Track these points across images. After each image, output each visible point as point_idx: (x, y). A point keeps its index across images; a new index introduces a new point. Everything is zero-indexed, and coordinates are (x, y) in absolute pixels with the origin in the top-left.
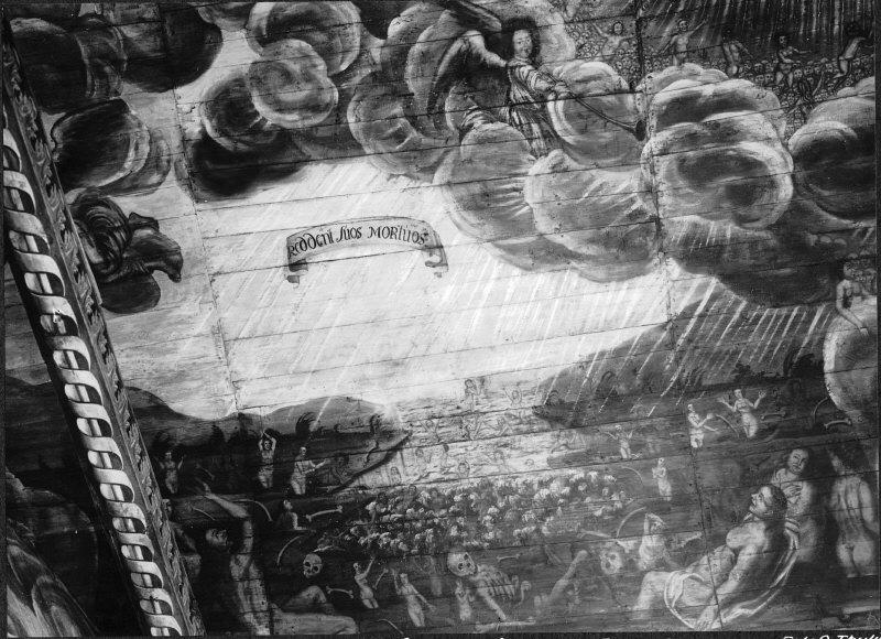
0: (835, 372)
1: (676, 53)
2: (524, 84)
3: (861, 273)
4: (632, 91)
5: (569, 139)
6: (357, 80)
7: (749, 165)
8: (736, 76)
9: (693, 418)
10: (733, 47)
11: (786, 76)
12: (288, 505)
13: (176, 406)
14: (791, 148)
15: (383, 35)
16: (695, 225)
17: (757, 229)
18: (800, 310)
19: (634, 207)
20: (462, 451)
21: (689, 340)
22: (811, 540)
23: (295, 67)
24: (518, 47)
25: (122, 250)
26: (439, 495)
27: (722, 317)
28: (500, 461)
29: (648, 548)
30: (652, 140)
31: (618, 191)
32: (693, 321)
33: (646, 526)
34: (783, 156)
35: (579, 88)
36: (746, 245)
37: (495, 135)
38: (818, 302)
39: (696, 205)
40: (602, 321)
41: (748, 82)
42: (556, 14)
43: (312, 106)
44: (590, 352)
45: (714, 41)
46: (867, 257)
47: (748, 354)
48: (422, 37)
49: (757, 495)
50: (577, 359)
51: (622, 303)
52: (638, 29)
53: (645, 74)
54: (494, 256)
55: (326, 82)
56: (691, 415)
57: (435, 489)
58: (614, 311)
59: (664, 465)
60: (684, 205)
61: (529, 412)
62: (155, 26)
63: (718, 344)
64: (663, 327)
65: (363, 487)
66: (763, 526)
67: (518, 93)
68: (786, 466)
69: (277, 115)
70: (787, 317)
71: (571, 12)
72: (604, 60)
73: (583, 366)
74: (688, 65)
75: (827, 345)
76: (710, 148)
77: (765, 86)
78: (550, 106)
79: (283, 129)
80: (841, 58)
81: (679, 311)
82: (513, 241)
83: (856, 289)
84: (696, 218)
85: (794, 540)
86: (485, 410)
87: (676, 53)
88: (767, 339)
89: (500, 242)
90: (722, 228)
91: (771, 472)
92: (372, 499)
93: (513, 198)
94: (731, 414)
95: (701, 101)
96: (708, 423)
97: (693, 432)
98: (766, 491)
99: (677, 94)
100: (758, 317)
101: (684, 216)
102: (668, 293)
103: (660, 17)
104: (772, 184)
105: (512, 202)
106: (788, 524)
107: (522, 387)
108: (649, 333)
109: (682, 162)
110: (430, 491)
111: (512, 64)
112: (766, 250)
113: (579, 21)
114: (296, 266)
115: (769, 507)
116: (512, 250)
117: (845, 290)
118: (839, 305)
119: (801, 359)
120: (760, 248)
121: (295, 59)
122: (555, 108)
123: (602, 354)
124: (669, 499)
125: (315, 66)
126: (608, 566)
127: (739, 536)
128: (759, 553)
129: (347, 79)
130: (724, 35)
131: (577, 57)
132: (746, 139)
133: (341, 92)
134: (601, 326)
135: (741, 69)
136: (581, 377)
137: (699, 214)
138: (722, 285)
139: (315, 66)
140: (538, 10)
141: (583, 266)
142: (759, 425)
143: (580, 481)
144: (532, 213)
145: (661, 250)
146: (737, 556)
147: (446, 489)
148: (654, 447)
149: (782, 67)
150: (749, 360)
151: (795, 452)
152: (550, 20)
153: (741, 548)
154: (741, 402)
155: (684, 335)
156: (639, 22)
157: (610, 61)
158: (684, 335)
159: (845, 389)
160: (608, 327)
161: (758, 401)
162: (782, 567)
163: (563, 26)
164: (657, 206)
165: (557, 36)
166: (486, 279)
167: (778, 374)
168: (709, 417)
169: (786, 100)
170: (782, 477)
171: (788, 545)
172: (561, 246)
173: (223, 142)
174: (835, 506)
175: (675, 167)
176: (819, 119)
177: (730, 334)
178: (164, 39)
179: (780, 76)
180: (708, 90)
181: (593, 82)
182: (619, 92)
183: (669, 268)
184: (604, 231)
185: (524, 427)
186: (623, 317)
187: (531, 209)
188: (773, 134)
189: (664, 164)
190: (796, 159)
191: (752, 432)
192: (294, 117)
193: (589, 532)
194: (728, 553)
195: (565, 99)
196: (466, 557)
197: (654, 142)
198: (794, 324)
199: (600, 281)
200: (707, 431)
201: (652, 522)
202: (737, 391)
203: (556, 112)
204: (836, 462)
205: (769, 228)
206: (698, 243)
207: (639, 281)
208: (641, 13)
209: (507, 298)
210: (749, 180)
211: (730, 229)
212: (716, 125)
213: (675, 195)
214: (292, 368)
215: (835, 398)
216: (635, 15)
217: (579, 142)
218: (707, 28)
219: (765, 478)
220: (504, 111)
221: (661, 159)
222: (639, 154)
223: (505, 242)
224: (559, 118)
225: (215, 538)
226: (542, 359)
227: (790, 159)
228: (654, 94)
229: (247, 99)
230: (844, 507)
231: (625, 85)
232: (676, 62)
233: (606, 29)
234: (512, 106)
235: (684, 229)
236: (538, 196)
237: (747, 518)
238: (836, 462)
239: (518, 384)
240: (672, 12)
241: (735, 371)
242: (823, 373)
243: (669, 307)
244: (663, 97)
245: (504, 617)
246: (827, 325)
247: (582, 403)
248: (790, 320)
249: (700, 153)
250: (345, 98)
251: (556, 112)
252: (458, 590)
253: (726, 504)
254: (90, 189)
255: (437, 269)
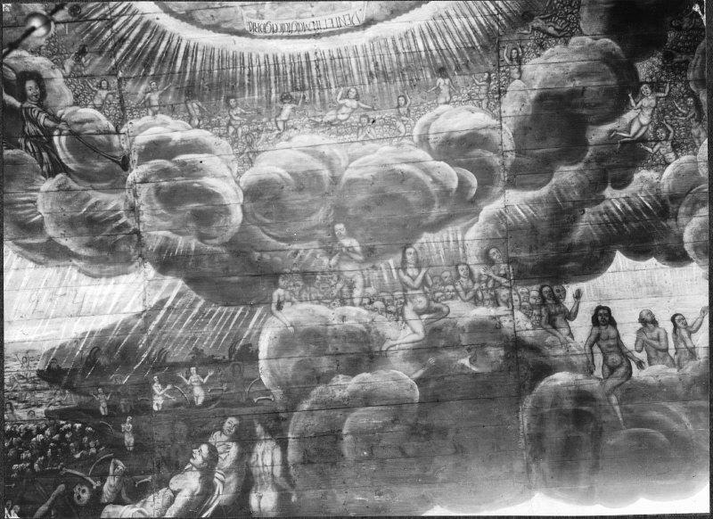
0: (268, 359)
1: (150, 106)
2: (35, 122)
3: (292, 284)
4: (117, 132)
5: (71, 166)
7: (207, 195)
8: (198, 127)
9: (157, 387)
10: (195, 105)
11: (236, 129)
14: (242, 185)
16: (167, 238)
17: (215, 245)
18: (244, 309)
19: (120, 222)
21: (159, 326)
22: (233, 487)
24: (29, 93)
27: (185, 310)
29: (111, 486)
30: (135, 171)
31: (109, 208)
32: (163, 312)
34: (236, 190)
35: (77, 128)
36: (206, 257)
37: (14, 158)
38: (259, 304)
39: (168, 224)
40: (94, 306)
41: (207, 132)
42: (57, 70)
44: (83, 330)
45: (179, 99)
46: (297, 272)
47: (202, 341)
49: (197, 450)
50: (73, 335)
51: (109, 295)
52: (119, 87)
53: (127, 121)
54: (16, 252)
56: (155, 384)
58: (103, 300)
59: (131, 422)
60: (160, 223)
61: (34, 374)
63: (181, 331)
64: (138, 316)
66: (198, 474)
67: (30, 128)
68: (222, 430)
70: (234, 314)
71: (68, 70)
72: (95, 107)
73: (77, 341)
74: (159, 116)
75: (261, 337)
76: (180, 181)
77: (220, 136)
78: (56, 139)
80: (278, 119)
81: (153, 303)
82: (29, 241)
83: (288, 297)
84: (168, 233)
85: (219, 487)
87: (150, 106)
88: (218, 330)
90: (186, 242)
91: (208, 434)
93: (29, 208)
94: (185, 386)
95: (172, 144)
96: (167, 392)
97: (155, 398)
98: (204, 448)
99: (154, 137)
100: (213, 312)
101: (157, 229)
102: (145, 289)
103: (136, 79)
104: (226, 211)
105: (27, 211)
106: (217, 475)
107: (30, 355)
108: (129, 320)
109: (158, 190)
111: (26, 105)
112: (221, 262)
113: (74, 77)
115: (205, 460)
116: (29, 247)
117: (279, 296)
118: (274, 307)
119: (243, 347)
120: (216, 260)
122: (60, 141)
123: (92, 333)
126: (79, 497)
127: (180, 481)
128: (192, 495)
130: (187, 95)
131: (76, 104)
132: (208, 176)
134: (92, 311)
135: (201, 122)
136: (75, 350)
137: (170, 230)
138: (186, 286)
140: (42, 66)
141: (81, 264)
142: (206, 395)
143: (67, 430)
144: (43, 220)
145: (140, 256)
146: (175, 497)
148: (125, 408)
149: (233, 122)
150: (202, 346)
151: (230, 419)
152: (53, 75)
153: (179, 491)
154: (194, 378)
155: (155, 323)
156: (120, 80)
157: (100, 109)
158: (155, 323)
159: (273, 372)
160: (98, 312)
161: (207, 378)
162: (207, 508)
163: (62, 80)
164: (139, 222)
165: (58, 87)
167: (224, 357)
168: (169, 387)
169: (237, 147)
170: (217, 438)
171: (214, 491)
172: (66, 247)
174: (254, 463)
175: (153, 193)
176: (262, 164)
177: (191, 324)
179: (231, 130)
180: (177, 137)
181: (87, 124)
182: (107, 133)
183: (147, 270)
184: (98, 238)
185: (29, 386)
186: (110, 304)
187: (43, 217)
188: (228, 173)
189: (144, 190)
190: (246, 194)
191: (200, 401)
193: (70, 471)
194: (169, 493)
195: (67, 135)
197: (135, 173)
198: (238, 322)
199: (94, 277)
200: (166, 399)
201: (116, 466)
202: (192, 368)
203: (61, 145)
204: (259, 429)
205: (224, 245)
206: (169, 253)
207: (123, 278)
208: (120, 74)
209: (23, 285)
210: (210, 207)
211: (194, 243)
212: (184, 164)
213: (152, 215)
215: (265, 379)
216: (116, 75)
217: (81, 169)
218: (172, 89)
219: (203, 437)
220: (21, 141)
221: (142, 186)
222: (125, 180)
223: (20, 241)
224: (62, 149)
226: (48, 333)
227: (241, 193)
228: (135, 136)
230: (261, 464)
231: (112, 128)
232: (150, 113)
233: (95, 84)
234: (28, 137)
235: (159, 241)
236: (48, 207)
237: (187, 467)
238: (259, 429)
239: (27, 352)
240: (145, 75)
241: (191, 353)
242: (258, 359)
243: (144, 300)
244: (143, 139)
246: (264, 322)
247: (74, 371)
248: (236, 316)
249: (172, 183)
251: (61, 145)
253: (173, 455)
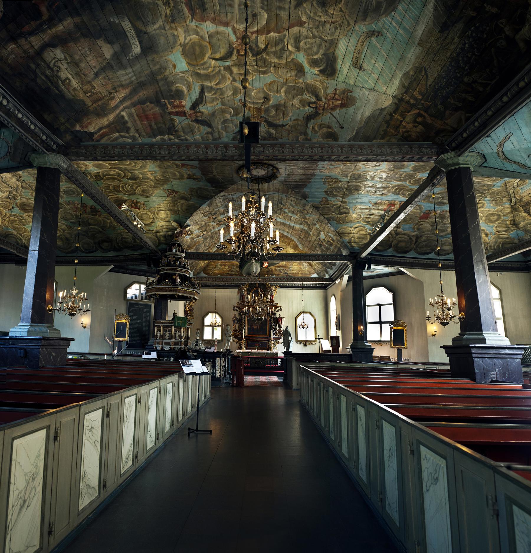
6: (316, 33)
12: (423, 102)
13: (384, 107)
15: (305, 23)
20: (438, 58)
23: (308, 46)
25: (340, 97)
26: (446, 71)
28: (448, 51)
33: (501, 26)
43: (320, 46)
48: (309, 13)
50: (432, 10)
55: (314, 40)
57: (444, 71)
62: (289, 70)
65: (430, 85)
69: (319, 54)
79: (323, 54)
86: (430, 45)
89: (381, 13)
92: (435, 86)
93: (368, 5)
105: (370, 5)
110: (443, 72)
114: (361, 68)
121: (306, 45)
124: (499, 12)
125: (309, 41)
129: (315, 35)
133: (318, 38)
139: (309, 41)
147: (445, 68)
166: (391, 23)
173: (321, 68)
178: (293, 70)
192: (321, 51)
193: (489, 42)
196: (468, 77)
201: (502, 23)
209: (400, 20)
214: (388, 81)
225: (419, 119)
229: (312, 59)
245: (490, 82)
250: (320, 37)
252: (474, 86)
254: (323, 96)
255: (380, 35)
